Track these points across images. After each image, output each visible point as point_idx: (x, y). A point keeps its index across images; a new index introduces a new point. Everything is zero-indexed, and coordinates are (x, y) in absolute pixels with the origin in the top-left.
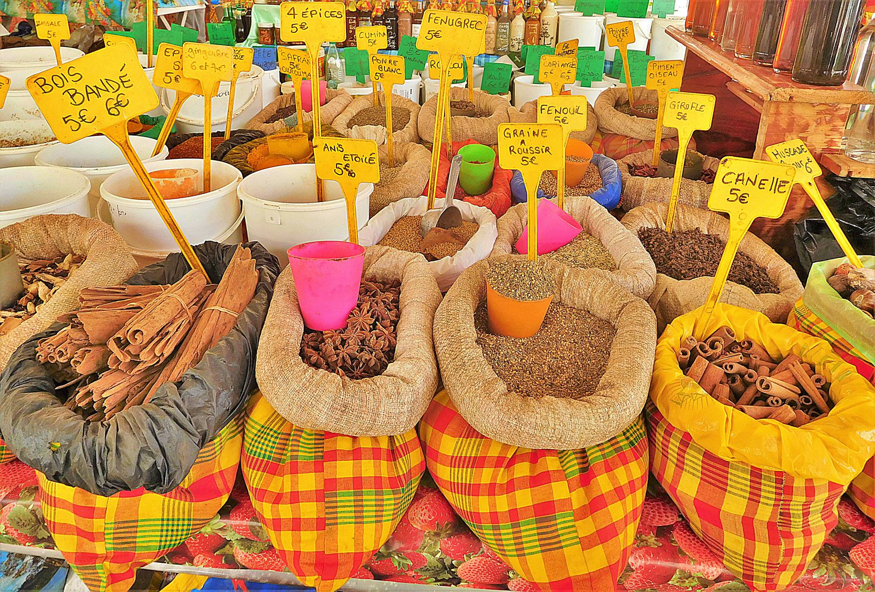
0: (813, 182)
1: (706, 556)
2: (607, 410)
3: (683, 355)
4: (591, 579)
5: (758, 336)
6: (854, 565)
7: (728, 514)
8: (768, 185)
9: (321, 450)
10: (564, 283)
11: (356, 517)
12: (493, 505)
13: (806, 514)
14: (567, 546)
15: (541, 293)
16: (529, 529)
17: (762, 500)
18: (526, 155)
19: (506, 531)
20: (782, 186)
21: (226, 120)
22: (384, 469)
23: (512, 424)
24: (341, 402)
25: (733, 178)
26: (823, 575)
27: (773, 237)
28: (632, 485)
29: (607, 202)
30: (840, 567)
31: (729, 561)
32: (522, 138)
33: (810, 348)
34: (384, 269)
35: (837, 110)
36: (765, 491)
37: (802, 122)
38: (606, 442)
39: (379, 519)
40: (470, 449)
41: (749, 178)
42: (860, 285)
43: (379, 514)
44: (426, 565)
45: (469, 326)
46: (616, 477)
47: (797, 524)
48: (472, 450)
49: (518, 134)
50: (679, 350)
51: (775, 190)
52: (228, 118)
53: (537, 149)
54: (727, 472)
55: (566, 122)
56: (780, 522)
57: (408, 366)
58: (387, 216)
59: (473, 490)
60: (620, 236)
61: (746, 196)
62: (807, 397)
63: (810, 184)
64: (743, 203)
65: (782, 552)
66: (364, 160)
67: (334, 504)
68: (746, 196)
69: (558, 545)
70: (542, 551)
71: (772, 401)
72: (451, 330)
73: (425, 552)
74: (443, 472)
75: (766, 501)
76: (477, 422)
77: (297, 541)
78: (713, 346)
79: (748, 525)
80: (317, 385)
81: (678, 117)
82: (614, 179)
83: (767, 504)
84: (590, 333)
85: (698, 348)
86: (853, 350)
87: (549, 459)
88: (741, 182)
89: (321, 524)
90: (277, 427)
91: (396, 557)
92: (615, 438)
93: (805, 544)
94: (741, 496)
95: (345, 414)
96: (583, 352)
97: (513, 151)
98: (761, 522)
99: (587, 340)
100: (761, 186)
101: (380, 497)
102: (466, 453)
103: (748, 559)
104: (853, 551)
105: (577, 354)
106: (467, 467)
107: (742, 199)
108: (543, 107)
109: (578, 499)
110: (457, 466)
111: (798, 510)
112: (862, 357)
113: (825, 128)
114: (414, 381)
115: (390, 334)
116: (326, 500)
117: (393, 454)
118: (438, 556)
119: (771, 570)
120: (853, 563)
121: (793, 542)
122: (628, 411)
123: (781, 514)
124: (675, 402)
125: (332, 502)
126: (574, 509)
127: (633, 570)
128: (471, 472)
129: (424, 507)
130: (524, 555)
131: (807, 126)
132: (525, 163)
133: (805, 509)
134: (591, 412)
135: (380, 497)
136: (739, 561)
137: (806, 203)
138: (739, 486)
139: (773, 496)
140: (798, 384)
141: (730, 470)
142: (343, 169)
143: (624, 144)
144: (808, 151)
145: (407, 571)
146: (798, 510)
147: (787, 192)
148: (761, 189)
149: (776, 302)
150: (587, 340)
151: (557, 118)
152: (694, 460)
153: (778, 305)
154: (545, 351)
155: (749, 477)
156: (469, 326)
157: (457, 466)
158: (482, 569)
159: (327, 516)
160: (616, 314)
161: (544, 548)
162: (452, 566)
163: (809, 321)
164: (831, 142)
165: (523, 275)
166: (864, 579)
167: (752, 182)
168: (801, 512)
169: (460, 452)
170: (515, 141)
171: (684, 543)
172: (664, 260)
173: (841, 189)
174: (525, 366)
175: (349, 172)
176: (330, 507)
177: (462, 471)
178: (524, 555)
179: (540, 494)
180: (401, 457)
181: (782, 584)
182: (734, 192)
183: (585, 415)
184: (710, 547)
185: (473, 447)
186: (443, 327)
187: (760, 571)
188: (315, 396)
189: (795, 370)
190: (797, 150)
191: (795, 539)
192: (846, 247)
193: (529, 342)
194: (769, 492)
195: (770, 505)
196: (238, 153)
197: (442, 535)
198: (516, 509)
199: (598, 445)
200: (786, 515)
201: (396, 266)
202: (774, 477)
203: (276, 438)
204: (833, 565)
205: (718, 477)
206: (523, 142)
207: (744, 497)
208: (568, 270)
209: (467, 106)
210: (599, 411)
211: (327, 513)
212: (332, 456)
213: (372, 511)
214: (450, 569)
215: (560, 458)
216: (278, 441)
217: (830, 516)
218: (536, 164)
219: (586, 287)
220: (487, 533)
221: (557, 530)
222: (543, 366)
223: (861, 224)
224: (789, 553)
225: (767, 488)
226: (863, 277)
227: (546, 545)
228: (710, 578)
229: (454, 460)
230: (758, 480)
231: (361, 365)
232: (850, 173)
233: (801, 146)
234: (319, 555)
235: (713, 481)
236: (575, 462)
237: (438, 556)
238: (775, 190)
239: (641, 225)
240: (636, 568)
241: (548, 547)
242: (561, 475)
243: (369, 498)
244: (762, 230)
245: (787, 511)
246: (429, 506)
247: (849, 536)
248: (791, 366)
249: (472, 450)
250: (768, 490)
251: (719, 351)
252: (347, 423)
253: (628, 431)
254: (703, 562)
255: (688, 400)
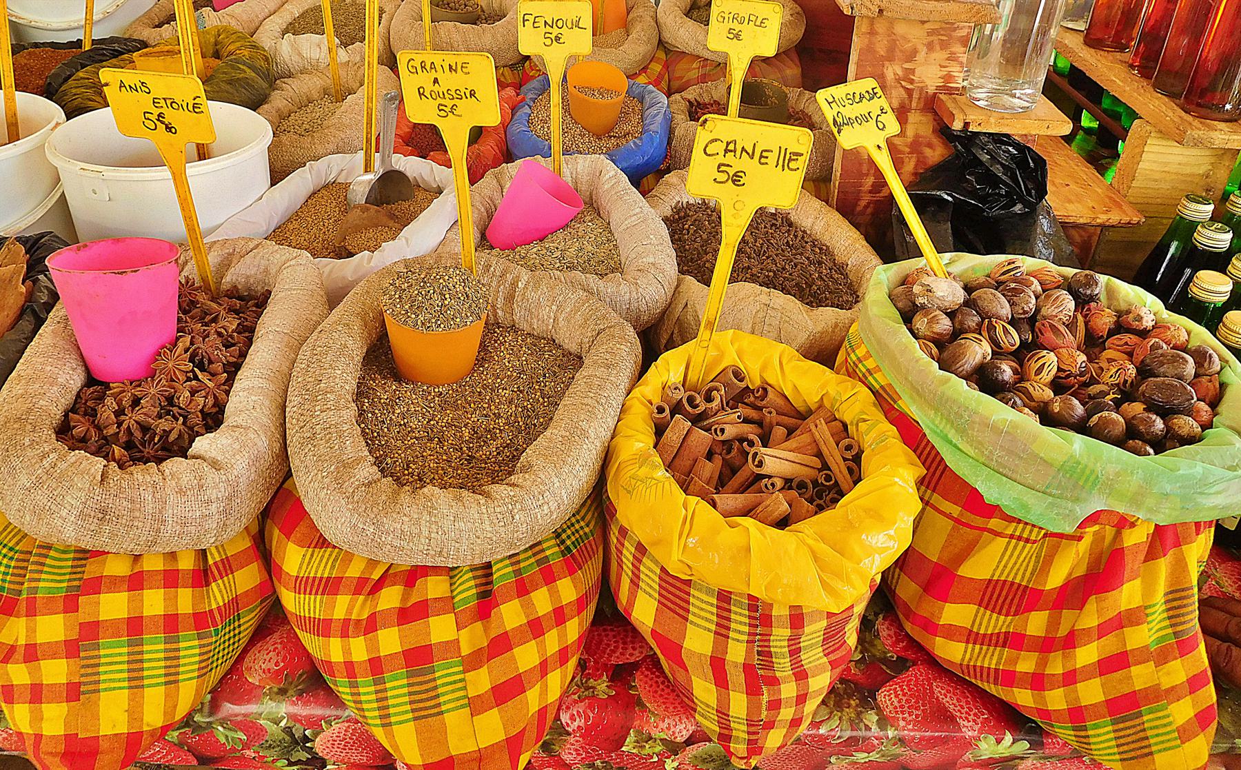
0: (883, 145)
1: (674, 708)
2: (510, 507)
3: (658, 413)
4: (480, 757)
5: (778, 381)
6: (879, 711)
7: (693, 653)
8: (772, 158)
9: (79, 576)
10: (518, 298)
11: (130, 679)
12: (347, 651)
13: (795, 652)
14: (448, 711)
15: (458, 320)
16: (398, 685)
17: (731, 634)
18: (443, 102)
19: (367, 690)
20: (794, 160)
21: (83, 23)
22: (185, 600)
23: (368, 532)
24: (94, 506)
25: (719, 147)
26: (835, 728)
27: (873, 214)
28: (560, 616)
29: (625, 165)
30: (859, 714)
31: (702, 716)
32: (433, 75)
33: (843, 400)
34: (248, 277)
35: (955, 30)
36: (736, 622)
37: (908, 46)
38: (526, 550)
39: (172, 678)
40: (321, 566)
41: (743, 148)
42: (926, 303)
43: (172, 670)
44: (267, 738)
45: (339, 372)
46: (533, 604)
47: (783, 666)
48: (325, 567)
49: (428, 67)
50: (657, 401)
51: (783, 166)
52: (86, 19)
53: (458, 92)
54: (689, 594)
55: (561, 41)
56: (760, 664)
57: (224, 441)
58: (299, 184)
59: (323, 628)
60: (633, 219)
61: (742, 174)
62: (829, 472)
63: (879, 147)
64: (738, 185)
65: (764, 702)
66: (185, 108)
67: (96, 661)
68: (742, 174)
69: (436, 710)
70: (415, 719)
71: (766, 485)
72: (310, 379)
73: (264, 719)
74: (290, 600)
75: (737, 636)
76: (325, 527)
77: (37, 718)
78: (709, 399)
79: (718, 666)
80: (60, 479)
81: (729, 36)
82: (656, 126)
83: (738, 641)
84: (545, 375)
85: (684, 401)
86: (899, 402)
87: (432, 580)
88: (733, 153)
89: (73, 692)
90: (15, 540)
91: (220, 728)
92: (539, 543)
93: (798, 690)
94: (705, 629)
95: (106, 523)
96: (529, 406)
97: (423, 94)
98: (736, 665)
99: (537, 387)
100: (763, 160)
101: (174, 646)
102: (316, 572)
103: (723, 713)
104: (883, 690)
105: (520, 409)
106: (316, 594)
107: (736, 179)
108: (526, 17)
109: (472, 638)
110: (302, 591)
111: (781, 647)
112: (909, 413)
113: (940, 55)
114: (229, 466)
115: (218, 387)
116: (82, 654)
117: (202, 577)
118: (283, 724)
119: (753, 729)
120: (878, 708)
121: (780, 690)
122: (546, 507)
123: (759, 653)
124: (626, 489)
125: (93, 657)
126: (463, 654)
127: (569, 734)
128: (321, 601)
129: (272, 648)
130: (390, 724)
131: (915, 52)
132: (443, 113)
133: (792, 645)
134: (485, 511)
135: (174, 646)
136: (712, 716)
137: (916, 165)
138: (703, 614)
139: (746, 629)
140: (819, 455)
141: (692, 592)
142: (156, 121)
143: (695, 69)
144: (883, 96)
145: (242, 750)
146: (781, 647)
147: (801, 168)
148: (763, 164)
149: (833, 321)
150: (537, 387)
151: (547, 35)
152: (649, 577)
153: (836, 325)
154: (472, 405)
155: (715, 602)
156: (339, 372)
157: (302, 591)
158: (351, 741)
159: (83, 679)
160: (588, 345)
161: (417, 714)
162: (306, 739)
163: (856, 356)
164: (949, 78)
165: (432, 291)
166: (889, 732)
167: (748, 154)
168: (787, 649)
169: (308, 570)
170: (425, 79)
171: (648, 688)
172: (699, 253)
173: (960, 147)
174: (433, 431)
175: (166, 125)
176: (88, 666)
177: (310, 599)
178: (390, 724)
179: (414, 634)
180: (215, 580)
181: (772, 746)
182: (723, 168)
183: (476, 516)
184: (681, 695)
185: (327, 563)
186: (300, 375)
187: (740, 730)
188: (54, 497)
189: (817, 433)
190: (867, 95)
191: (782, 686)
192: (923, 244)
193: (451, 392)
194: (741, 623)
195: (741, 642)
196: (88, 79)
197: (291, 692)
198: (379, 657)
199: (510, 557)
200: (766, 654)
201: (266, 271)
202: (747, 601)
203: (11, 559)
204: (849, 713)
205: (678, 601)
206: (436, 81)
207: (709, 630)
208: (525, 275)
209: (466, 6)
210: (498, 510)
211: (82, 676)
212: (95, 586)
213: (160, 668)
214: (304, 744)
215: (451, 578)
216: (13, 564)
217: (841, 645)
218: (459, 116)
219: (549, 304)
220: (342, 688)
221: (436, 688)
222: (463, 429)
223: (982, 200)
224: (775, 705)
225: (738, 618)
226: (930, 291)
227: (421, 709)
228: (679, 740)
229: (298, 582)
230: (726, 605)
231: (156, 439)
232: (967, 124)
233: (873, 89)
234: (70, 738)
235: (672, 606)
236: (472, 583)
237: (283, 724)
238: (783, 166)
239: (678, 198)
240: (574, 730)
241: (423, 713)
242: (447, 604)
243: (154, 647)
244: (856, 205)
245: (766, 649)
246: (279, 646)
247: (884, 667)
248: (813, 428)
249: (325, 567)
250: (740, 620)
251: (715, 404)
252: (112, 535)
253: (564, 531)
254: (668, 717)
255: (641, 487)
